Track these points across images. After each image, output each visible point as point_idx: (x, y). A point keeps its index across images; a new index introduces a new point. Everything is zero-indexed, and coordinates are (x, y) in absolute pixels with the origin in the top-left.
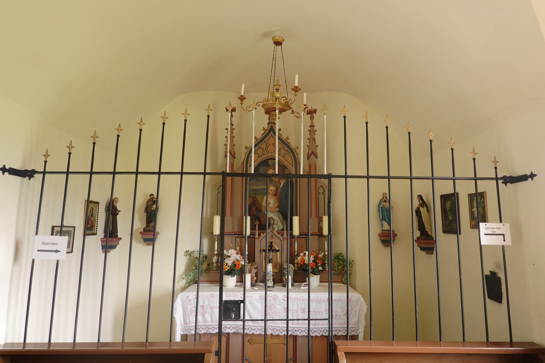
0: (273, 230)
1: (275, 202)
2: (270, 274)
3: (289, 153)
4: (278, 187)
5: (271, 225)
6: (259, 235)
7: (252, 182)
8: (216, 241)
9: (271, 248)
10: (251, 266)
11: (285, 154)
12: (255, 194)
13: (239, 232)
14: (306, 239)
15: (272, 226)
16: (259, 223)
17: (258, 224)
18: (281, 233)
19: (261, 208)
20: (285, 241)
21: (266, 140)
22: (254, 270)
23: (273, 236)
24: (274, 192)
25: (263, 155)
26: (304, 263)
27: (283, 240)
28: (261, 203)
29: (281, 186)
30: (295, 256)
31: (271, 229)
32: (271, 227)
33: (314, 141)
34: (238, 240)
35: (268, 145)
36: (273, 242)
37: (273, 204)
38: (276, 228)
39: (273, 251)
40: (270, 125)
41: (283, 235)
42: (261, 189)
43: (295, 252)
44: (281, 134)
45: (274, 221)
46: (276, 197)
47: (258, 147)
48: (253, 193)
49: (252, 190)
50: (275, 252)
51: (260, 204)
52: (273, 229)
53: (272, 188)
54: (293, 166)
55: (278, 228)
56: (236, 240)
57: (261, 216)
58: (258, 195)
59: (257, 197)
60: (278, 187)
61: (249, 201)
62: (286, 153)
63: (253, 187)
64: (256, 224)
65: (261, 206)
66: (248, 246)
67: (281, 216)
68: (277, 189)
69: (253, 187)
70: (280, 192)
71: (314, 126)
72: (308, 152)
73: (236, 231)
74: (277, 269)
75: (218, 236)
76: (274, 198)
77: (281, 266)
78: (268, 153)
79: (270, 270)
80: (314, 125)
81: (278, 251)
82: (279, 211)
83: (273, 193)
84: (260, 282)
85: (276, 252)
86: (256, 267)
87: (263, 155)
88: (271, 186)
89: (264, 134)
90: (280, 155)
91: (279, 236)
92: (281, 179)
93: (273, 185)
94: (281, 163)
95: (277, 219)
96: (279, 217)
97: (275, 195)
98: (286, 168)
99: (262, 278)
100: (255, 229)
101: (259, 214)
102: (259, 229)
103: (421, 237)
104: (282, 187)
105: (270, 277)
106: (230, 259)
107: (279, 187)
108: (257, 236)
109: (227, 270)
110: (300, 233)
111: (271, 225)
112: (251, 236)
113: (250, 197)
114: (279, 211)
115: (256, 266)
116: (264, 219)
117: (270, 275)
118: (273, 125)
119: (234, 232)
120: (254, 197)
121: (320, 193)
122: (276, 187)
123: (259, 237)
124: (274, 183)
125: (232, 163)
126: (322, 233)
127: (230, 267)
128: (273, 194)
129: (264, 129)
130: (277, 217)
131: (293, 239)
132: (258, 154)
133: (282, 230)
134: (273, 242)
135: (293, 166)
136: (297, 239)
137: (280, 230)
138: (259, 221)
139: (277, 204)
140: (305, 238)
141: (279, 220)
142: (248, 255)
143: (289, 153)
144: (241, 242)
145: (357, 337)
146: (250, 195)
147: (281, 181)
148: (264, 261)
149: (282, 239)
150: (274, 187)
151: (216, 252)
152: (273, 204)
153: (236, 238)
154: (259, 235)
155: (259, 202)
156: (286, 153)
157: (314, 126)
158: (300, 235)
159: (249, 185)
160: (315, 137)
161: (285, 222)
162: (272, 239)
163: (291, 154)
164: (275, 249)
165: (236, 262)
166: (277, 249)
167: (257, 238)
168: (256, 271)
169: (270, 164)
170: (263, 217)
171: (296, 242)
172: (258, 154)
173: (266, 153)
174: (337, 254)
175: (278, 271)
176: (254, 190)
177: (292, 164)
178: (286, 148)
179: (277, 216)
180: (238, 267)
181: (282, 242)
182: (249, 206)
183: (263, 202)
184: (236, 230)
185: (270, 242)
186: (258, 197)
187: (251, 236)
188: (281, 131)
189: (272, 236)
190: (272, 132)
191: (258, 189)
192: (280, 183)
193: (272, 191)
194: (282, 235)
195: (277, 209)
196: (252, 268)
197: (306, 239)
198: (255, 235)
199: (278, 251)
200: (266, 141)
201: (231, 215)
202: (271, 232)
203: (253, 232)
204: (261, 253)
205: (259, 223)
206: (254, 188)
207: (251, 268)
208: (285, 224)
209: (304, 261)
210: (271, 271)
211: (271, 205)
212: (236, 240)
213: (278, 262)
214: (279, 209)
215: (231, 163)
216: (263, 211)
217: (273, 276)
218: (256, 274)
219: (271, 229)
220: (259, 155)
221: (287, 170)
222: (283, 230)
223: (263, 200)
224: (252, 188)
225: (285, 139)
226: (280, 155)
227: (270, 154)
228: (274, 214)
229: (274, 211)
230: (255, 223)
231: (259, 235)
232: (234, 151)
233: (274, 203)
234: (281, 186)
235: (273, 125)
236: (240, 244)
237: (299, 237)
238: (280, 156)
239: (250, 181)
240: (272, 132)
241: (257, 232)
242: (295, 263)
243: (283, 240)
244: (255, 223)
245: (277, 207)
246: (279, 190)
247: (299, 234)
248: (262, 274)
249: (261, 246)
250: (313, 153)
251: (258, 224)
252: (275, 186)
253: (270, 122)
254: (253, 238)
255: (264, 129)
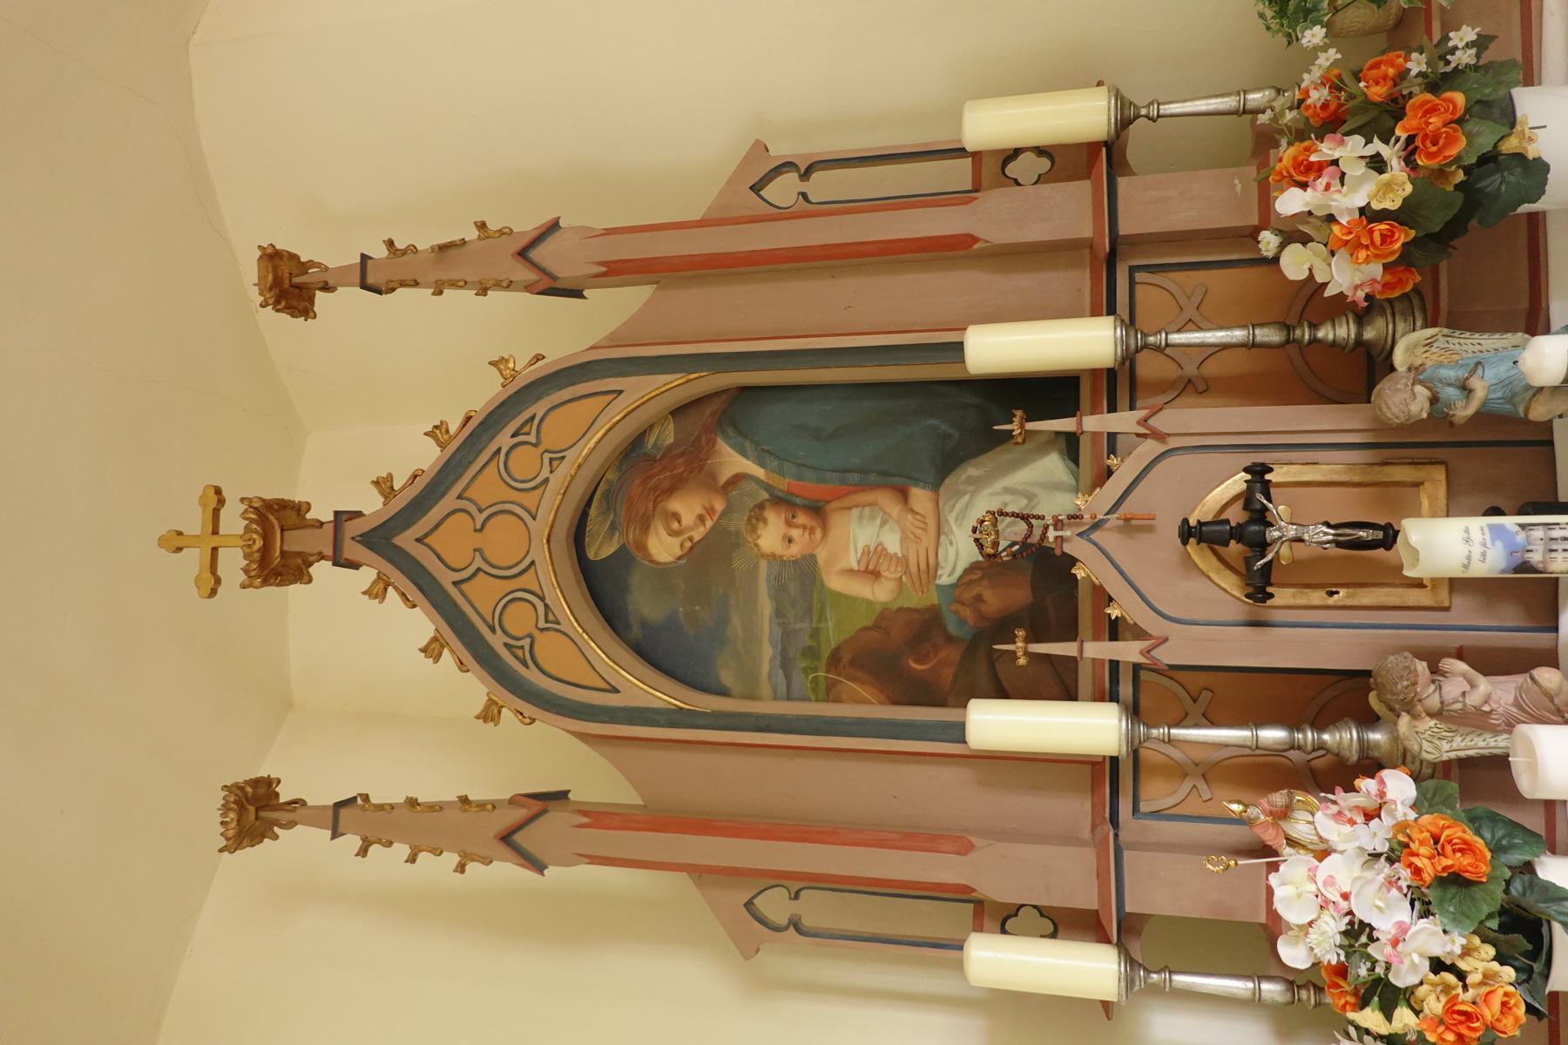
0: (1075, 517)
1: (867, 511)
2: (1521, 537)
3: (533, 418)
4: (766, 496)
5: (1037, 533)
6: (1115, 630)
7: (727, 678)
8: (1176, 978)
9: (1238, 533)
10: (1415, 717)
11: (542, 448)
12: (811, 653)
13: (1095, 785)
14: (1139, 277)
15: (1046, 528)
16: (1021, 633)
17: (1027, 640)
18: (1096, 457)
19: (909, 609)
20: (1161, 422)
21: (446, 578)
22: (1452, 688)
23: (1127, 520)
24: (802, 519)
25: (542, 599)
26: (1400, 216)
27: (1159, 436)
28: (878, 609)
29: (759, 472)
30: (1288, 342)
31: (1067, 533)
32: (1052, 534)
33: (452, 252)
34: (1157, 794)
35: (478, 563)
36: (1185, 521)
37: (884, 523)
38: (1054, 505)
39: (1261, 517)
40: (352, 550)
41: (1112, 437)
42: (779, 613)
43: (1254, 345)
44: (409, 474)
45: (1001, 513)
46: (834, 505)
47: (493, 629)
48: (806, 671)
49: (788, 676)
50: (1270, 500)
51: (885, 618)
52: (1070, 517)
53: (772, 536)
54: (620, 392)
55: (1056, 486)
56: (1157, 815)
57: (967, 612)
58: (815, 634)
59: (833, 645)
60: (766, 496)
61: (862, 701)
62: (532, 439)
63: (765, 668)
64: (1026, 653)
65: (901, 610)
66: (1213, 723)
67: (972, 470)
68: (781, 501)
69: (765, 668)
70: (800, 478)
71: (364, 258)
72: (529, 288)
73: (1088, 806)
74: (1417, 485)
75: (1131, 962)
76: (837, 521)
77: (1351, 466)
78: (533, 563)
79: (1476, 536)
80: (358, 260)
81: (1258, 472)
82: (936, 486)
83: (804, 527)
84: (1556, 630)
85: (1272, 491)
86: (1425, 664)
87: (542, 599)
88: (757, 545)
89: (403, 595)
90: (546, 480)
91: (1125, 471)
92: (713, 477)
93: (754, 529)
94: (610, 476)
95: (992, 494)
96: (978, 483)
97: (818, 511)
98: (638, 441)
99: (1510, 615)
100: (1071, 663)
101: (952, 628)
102: (1069, 632)
103: (1092, 177)
104: (762, 465)
105: (1556, 533)
106: (1384, 926)
107: (767, 487)
108: (1128, 651)
109: (1509, 973)
110: (1095, 312)
111: (1037, 533)
112: (1126, 690)
113: (831, 694)
114: (936, 486)
115: (1422, 666)
116: (988, 595)
117: (1538, 533)
118: (353, 528)
119: (1094, 827)
120: (834, 660)
121: (804, 195)
122: (761, 507)
123: (1139, 633)
124: (738, 522)
125: (585, 820)
126: (1092, 148)
127: (1477, 941)
128: (812, 531)
129: (377, 592)
130: (974, 494)
131: (1148, 367)
132: (537, 634)
133: (1076, 461)
134: (1185, 521)
135: (620, 392)
136: (1145, 335)
137: (1077, 480)
138: (1002, 628)
139: (886, 500)
140: (1132, 283)
141: (999, 485)
142: (1293, 725)
143: (533, 418)
144: (1176, 772)
145: (753, 907)
146: (822, 693)
147: (725, 475)
148: (1343, 592)
149: (1150, 448)
150: (765, 521)
151: (1266, 986)
152: (884, 523)
153: (1144, 807)
154: (1114, 636)
155: (866, 629)
156: (532, 439)
157: (364, 258)
158: (1111, 311)
159: (751, 696)
160: (428, 247)
161: (1014, 427)
162: (1149, 529)
163: (539, 408)
164: (1247, 498)
165: (1417, 872)
166: (1238, 482)
167: (1146, 652)
168: (1462, 666)
169: (612, 550)
170: (979, 599)
171: (1176, 338)
172: (537, 634)
173: (528, 581)
174: (1262, 16)
175: (1439, 474)
176: (786, 663)
177: (612, 396)
178: (504, 440)
179: (967, 497)
180: (1466, 848)
181: (1174, 443)
182: (895, 703)
183: (869, 602)
184: (1077, 809)
185: (1185, 542)
186: (834, 633)
187: (1126, 690)
188: (390, 476)
189: (1130, 526)
190: (398, 541)
191: (778, 633)
192: (738, 478)
193: (795, 533)
194: (1112, 450)
195: (920, 497)
196: (1434, 702)
197: (1139, 277)
198: (1115, 665)
199: (1258, 472)
200: (458, 576)
201: (965, 848)
202: (1095, 536)
203: (1096, 677)
204: (1279, 616)
205: (1021, 633)
206: (771, 660)
207: (1432, 715)
208: (1030, 426)
209: (1383, 215)
210: (1492, 528)
211: (893, 543)
212: (1157, 815)
213: (1356, 479)
214: (917, 481)
215: (581, 826)
216: (936, 601)
217: (1496, 511)
218: (1490, 662)
219: (1067, 533)
220: (542, 624)
221: (656, 432)
222: (1070, 445)
223: (853, 600)
224: (770, 676)
225: (442, 446)
226: (546, 480)
227: (540, 553)
228: (951, 518)
229: (932, 522)
230: (1022, 661)
231: (1115, 630)
232: (513, 801)
233: (873, 518)
234: (759, 472)
235: (353, 528)
236: (1187, 786)
237: (1125, 314)
238: (552, 477)
239: (723, 692)
240: (398, 541)
241: (1098, 650)
242: (1359, 334)
243: (1159, 436)
244: (1022, 661)
245: (903, 494)
246: (782, 484)
247: (1108, 321)
248: (1464, 610)
249: (1218, 618)
250: (522, 254)
251: (1027, 640)
252: (757, 515)
253: (329, 552)
254: (1144, 675)
255: (377, 592)
